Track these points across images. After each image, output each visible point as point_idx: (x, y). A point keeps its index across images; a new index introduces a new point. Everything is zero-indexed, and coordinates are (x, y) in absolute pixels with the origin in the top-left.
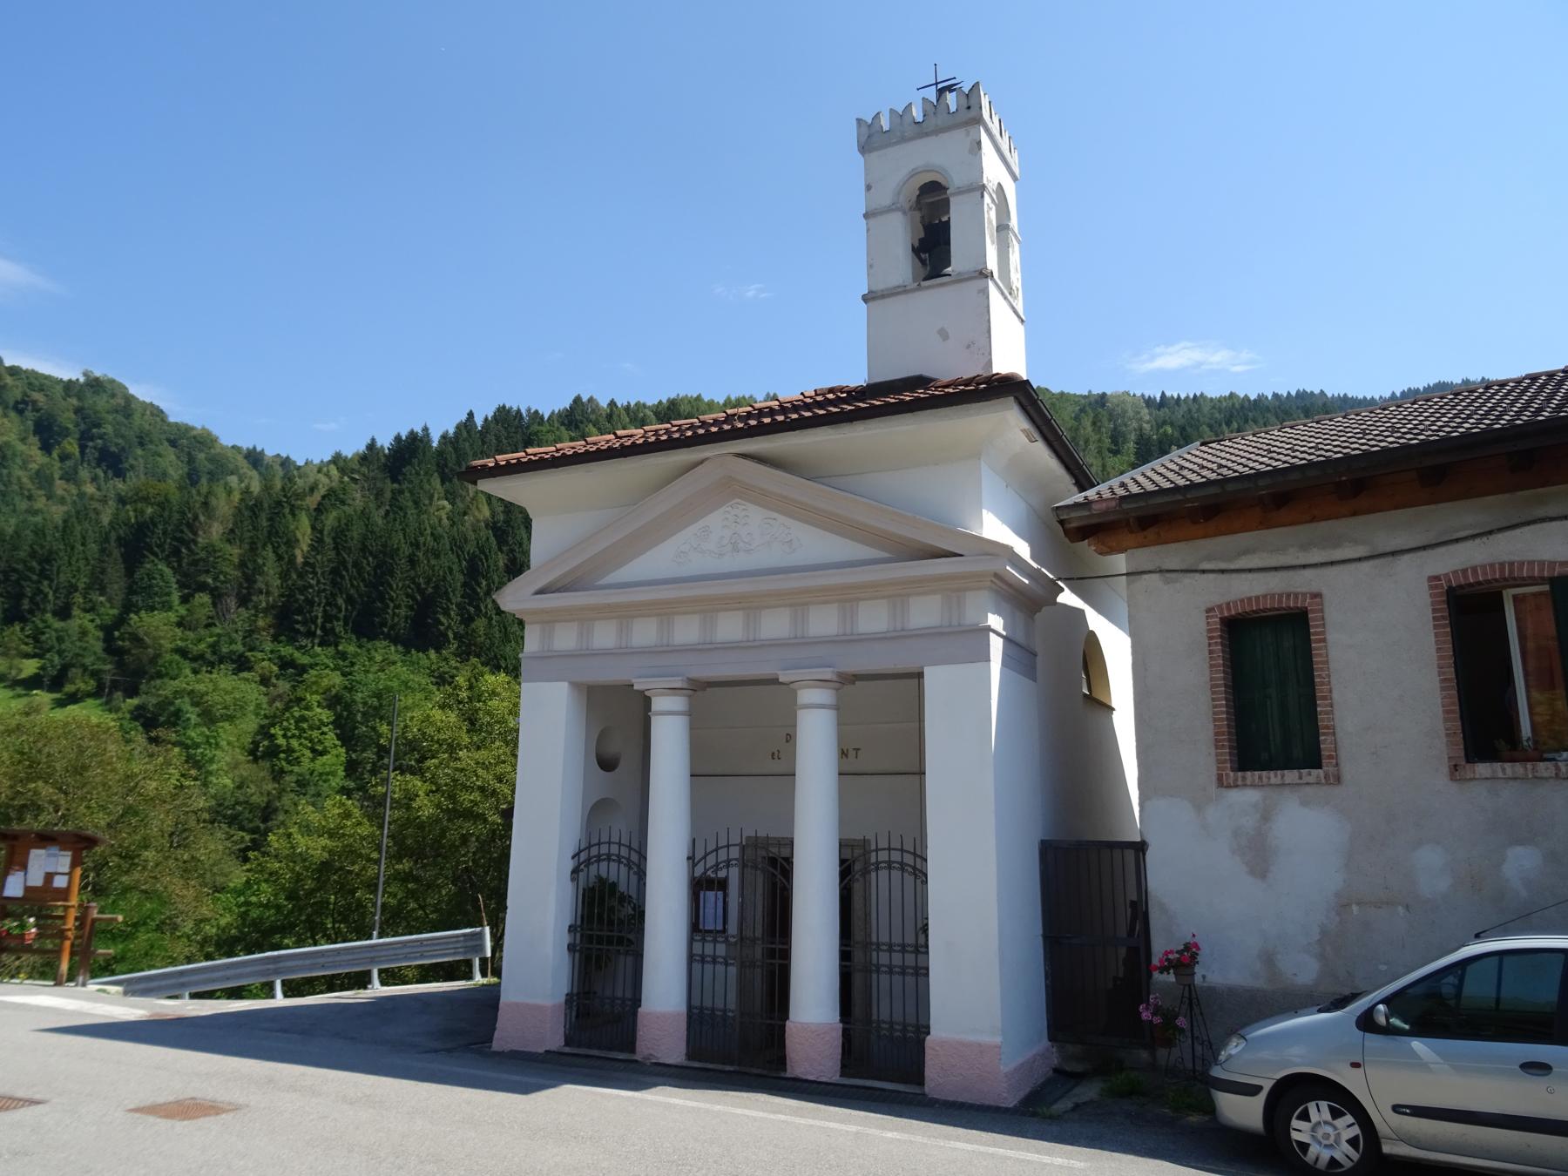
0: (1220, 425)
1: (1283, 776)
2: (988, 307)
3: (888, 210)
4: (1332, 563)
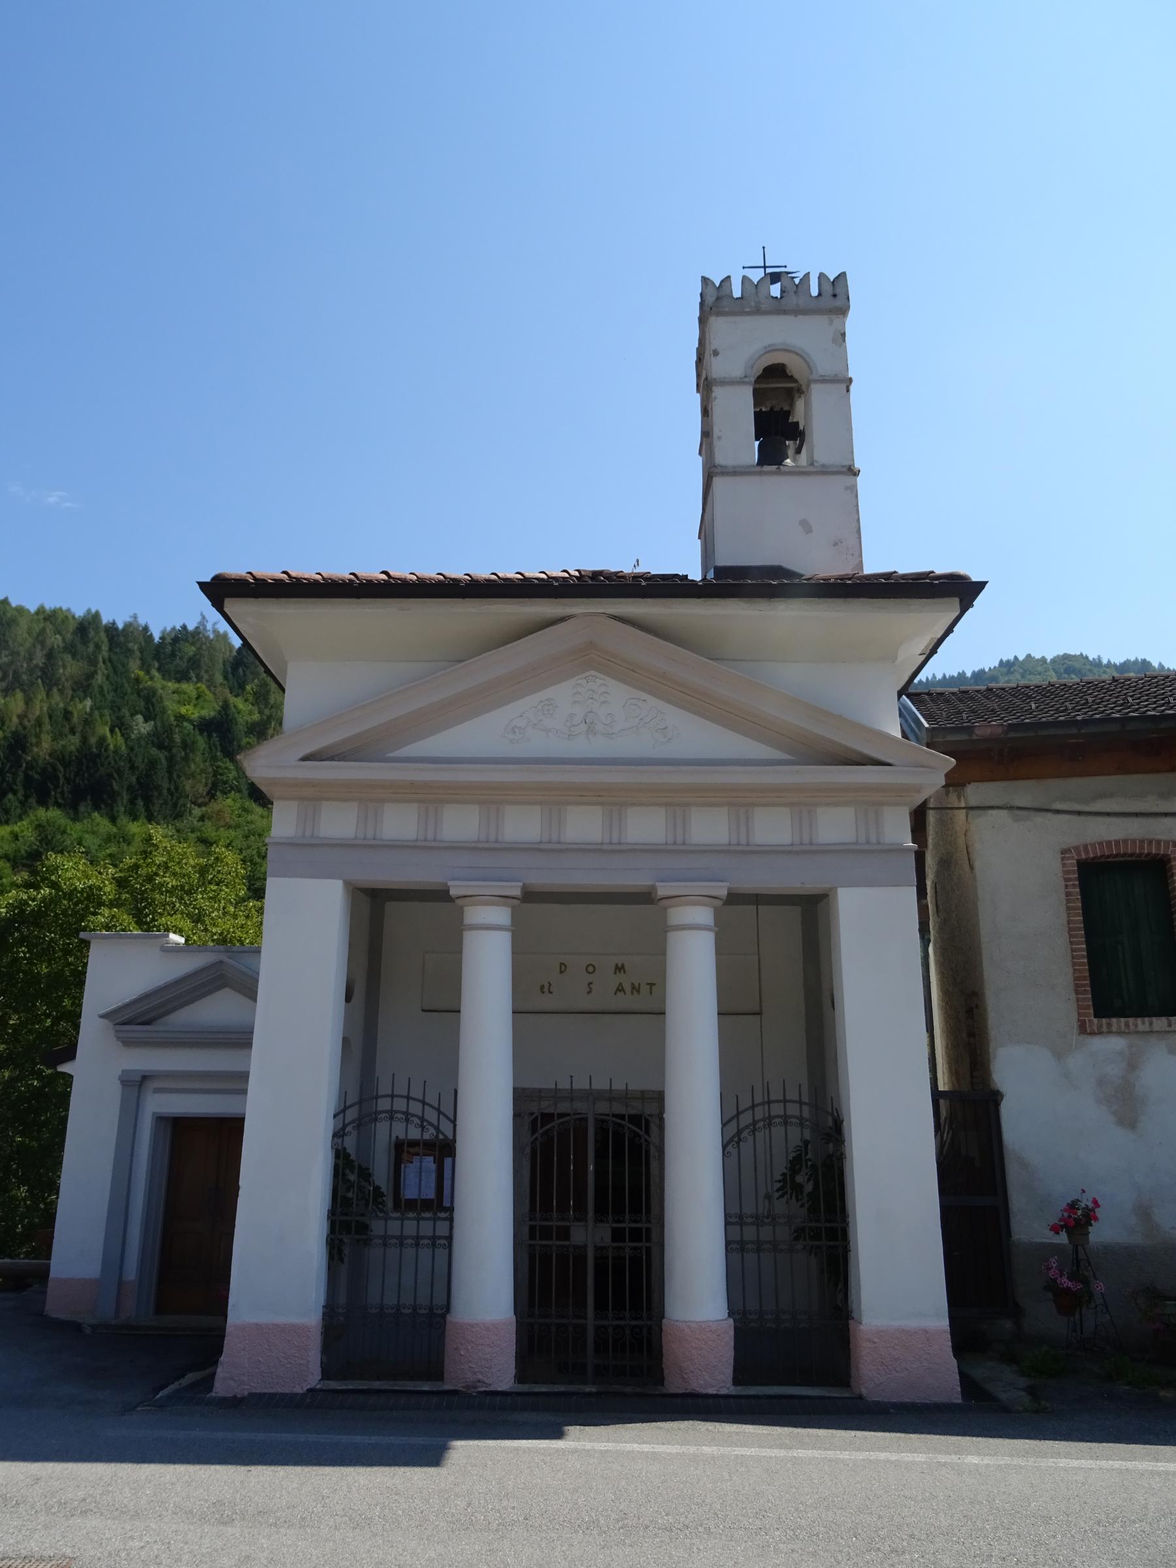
1: (1151, 1024)
2: (857, 505)
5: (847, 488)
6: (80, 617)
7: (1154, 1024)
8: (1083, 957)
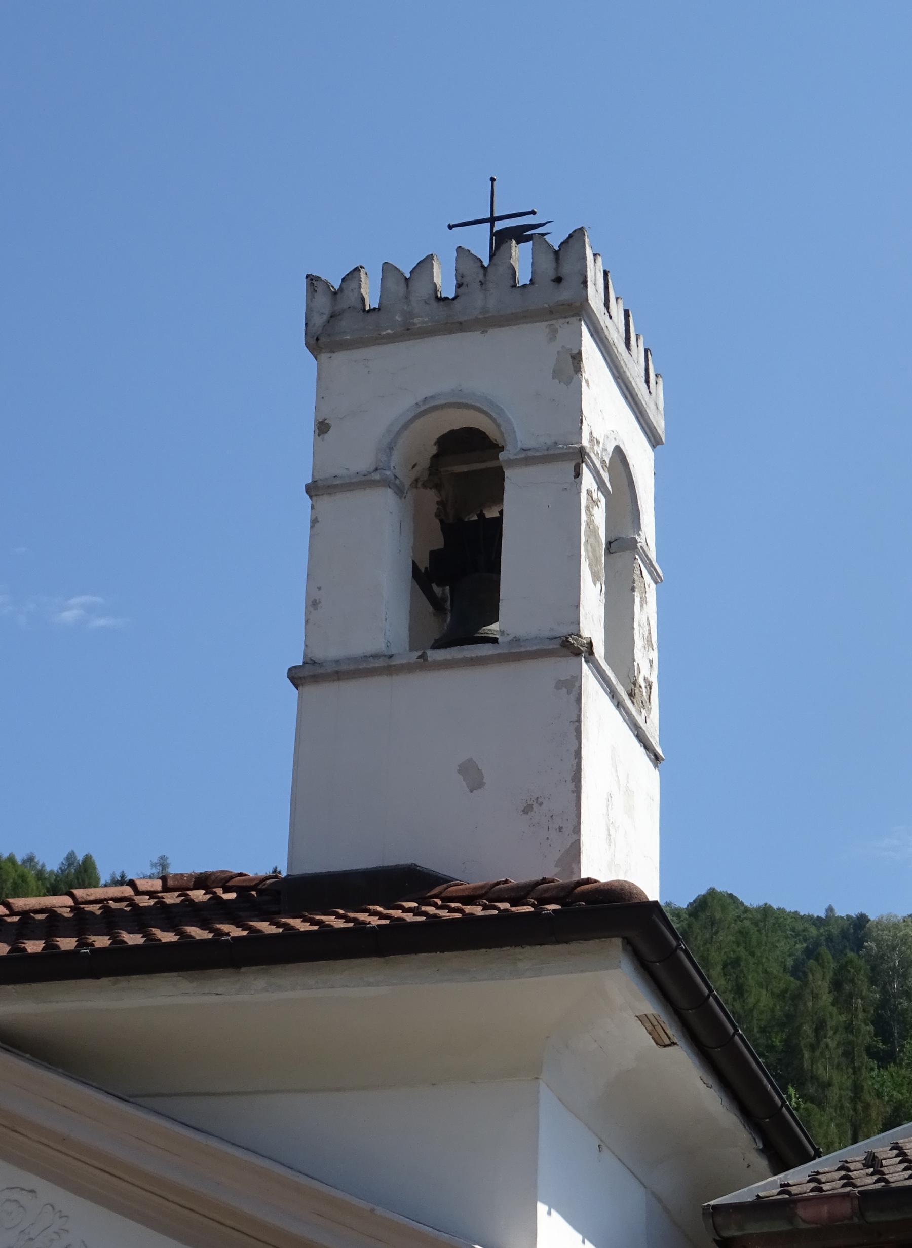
2: (579, 721)
3: (363, 482)
6: (52, 872)
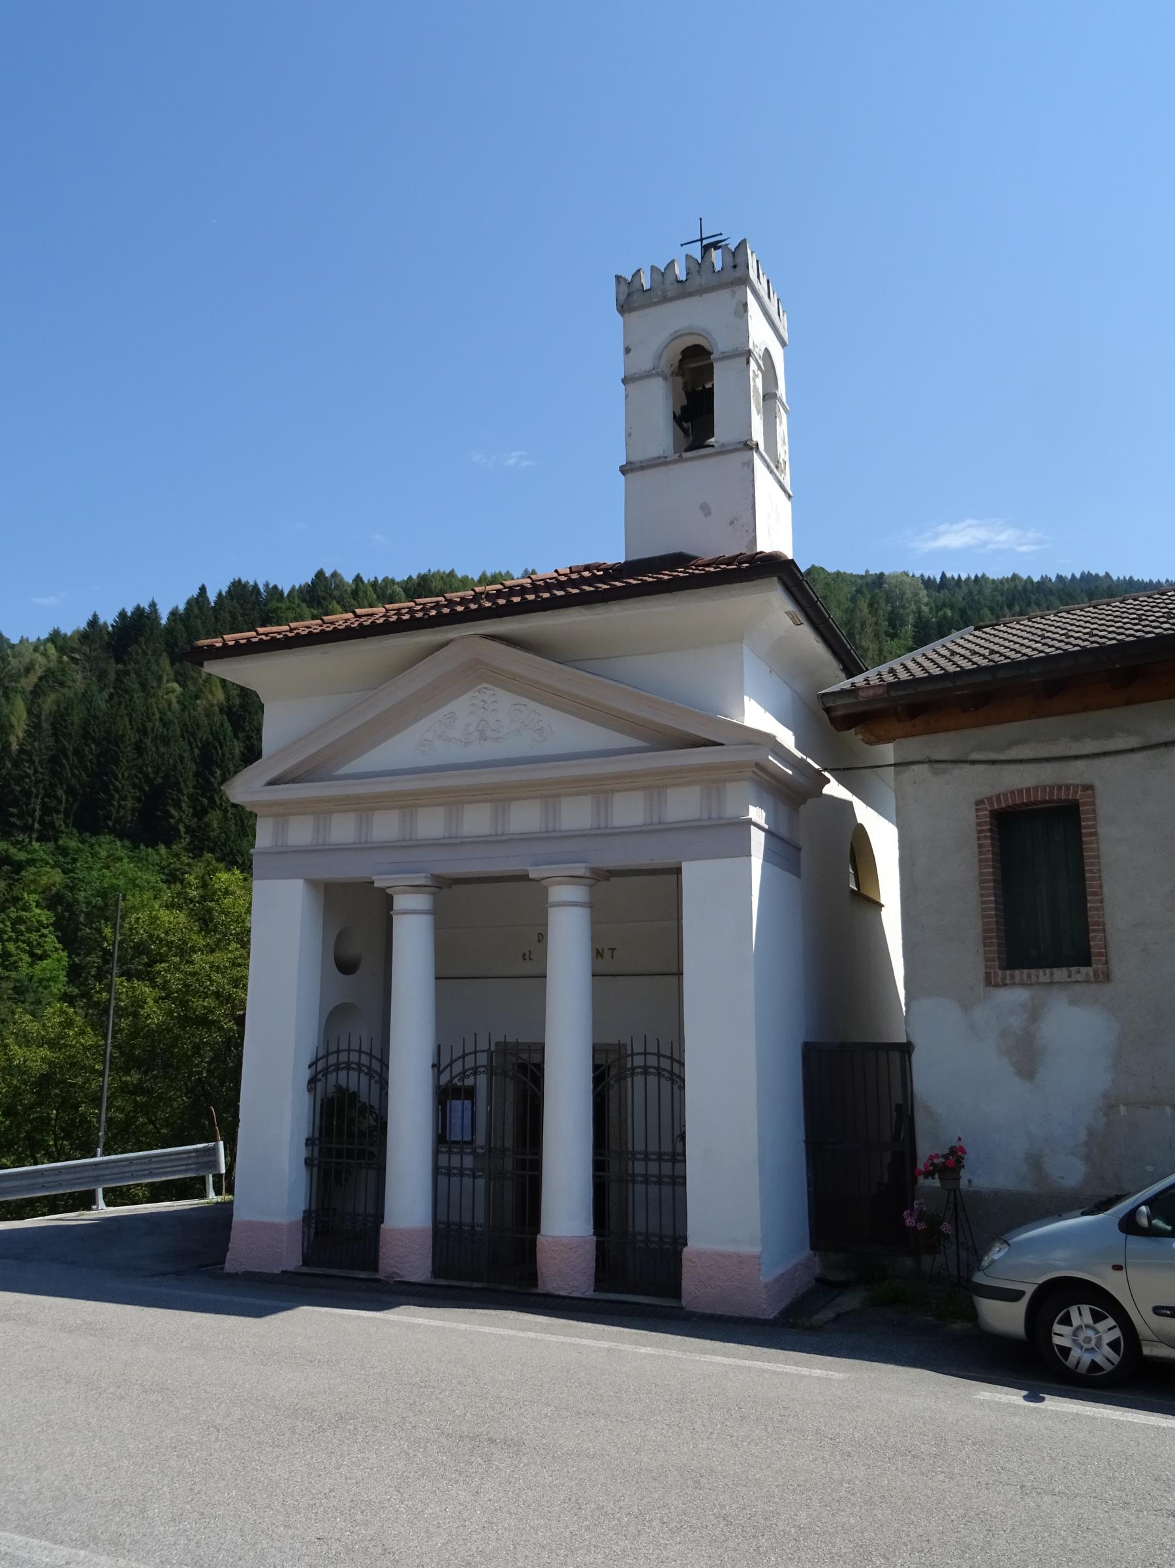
0: (1002, 608)
1: (1052, 974)
2: (753, 480)
4: (1105, 754)
5: (744, 464)
7: (1055, 975)
8: (991, 909)
